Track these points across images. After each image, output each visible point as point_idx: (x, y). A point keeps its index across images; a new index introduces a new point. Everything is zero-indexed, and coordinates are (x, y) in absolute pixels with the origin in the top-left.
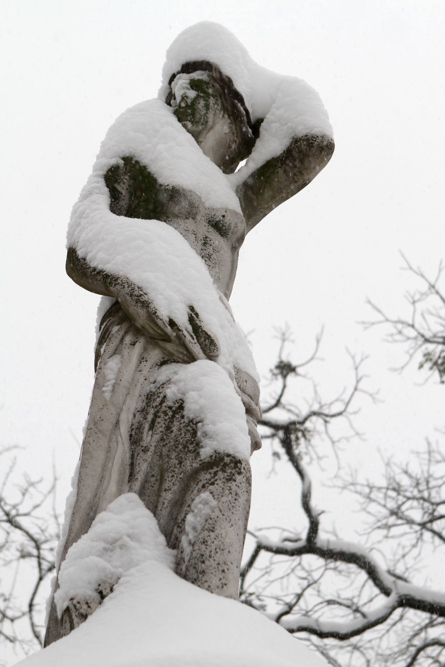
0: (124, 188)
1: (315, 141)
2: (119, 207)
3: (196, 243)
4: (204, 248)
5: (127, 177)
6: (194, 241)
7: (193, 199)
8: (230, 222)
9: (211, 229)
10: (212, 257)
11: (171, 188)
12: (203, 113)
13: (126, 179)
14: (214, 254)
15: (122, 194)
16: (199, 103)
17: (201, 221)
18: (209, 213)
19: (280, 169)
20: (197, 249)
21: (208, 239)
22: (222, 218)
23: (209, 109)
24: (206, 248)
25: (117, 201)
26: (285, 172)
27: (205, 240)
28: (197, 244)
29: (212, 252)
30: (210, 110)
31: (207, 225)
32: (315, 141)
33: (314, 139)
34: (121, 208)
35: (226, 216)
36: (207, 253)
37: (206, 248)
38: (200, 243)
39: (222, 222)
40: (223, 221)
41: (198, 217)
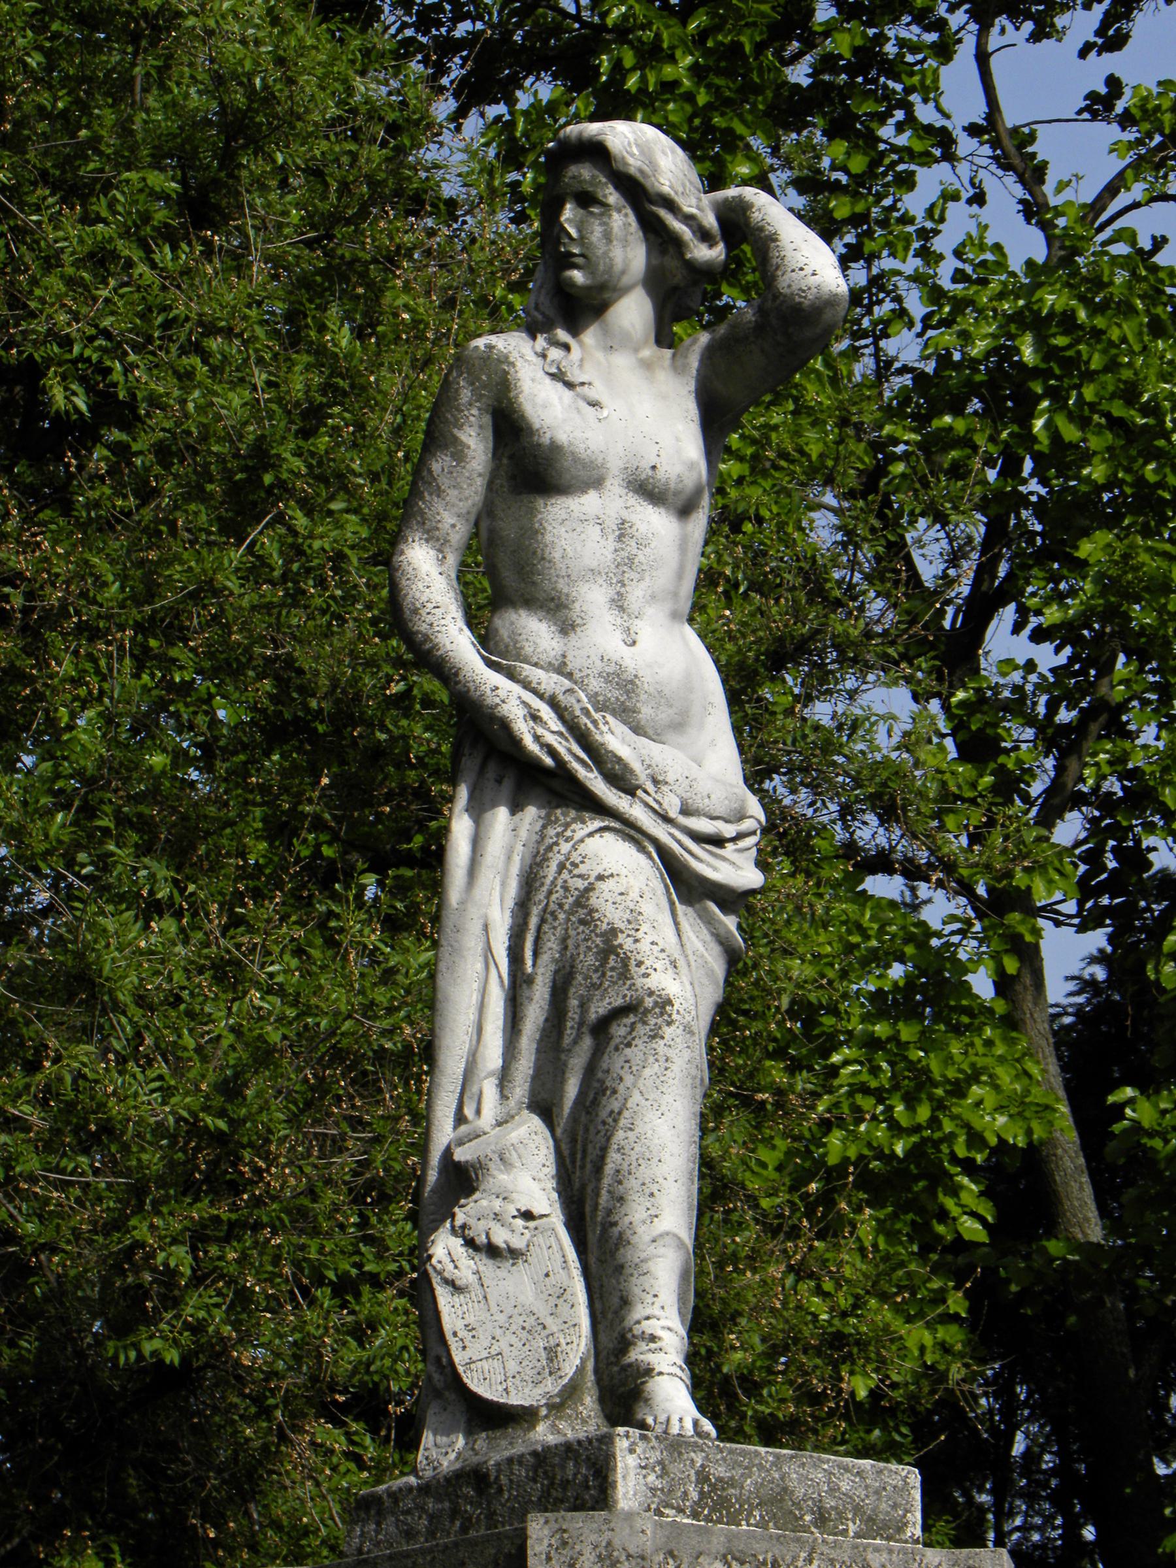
5: (474, 412)
9: (633, 500)
38: (611, 538)
41: (608, 483)
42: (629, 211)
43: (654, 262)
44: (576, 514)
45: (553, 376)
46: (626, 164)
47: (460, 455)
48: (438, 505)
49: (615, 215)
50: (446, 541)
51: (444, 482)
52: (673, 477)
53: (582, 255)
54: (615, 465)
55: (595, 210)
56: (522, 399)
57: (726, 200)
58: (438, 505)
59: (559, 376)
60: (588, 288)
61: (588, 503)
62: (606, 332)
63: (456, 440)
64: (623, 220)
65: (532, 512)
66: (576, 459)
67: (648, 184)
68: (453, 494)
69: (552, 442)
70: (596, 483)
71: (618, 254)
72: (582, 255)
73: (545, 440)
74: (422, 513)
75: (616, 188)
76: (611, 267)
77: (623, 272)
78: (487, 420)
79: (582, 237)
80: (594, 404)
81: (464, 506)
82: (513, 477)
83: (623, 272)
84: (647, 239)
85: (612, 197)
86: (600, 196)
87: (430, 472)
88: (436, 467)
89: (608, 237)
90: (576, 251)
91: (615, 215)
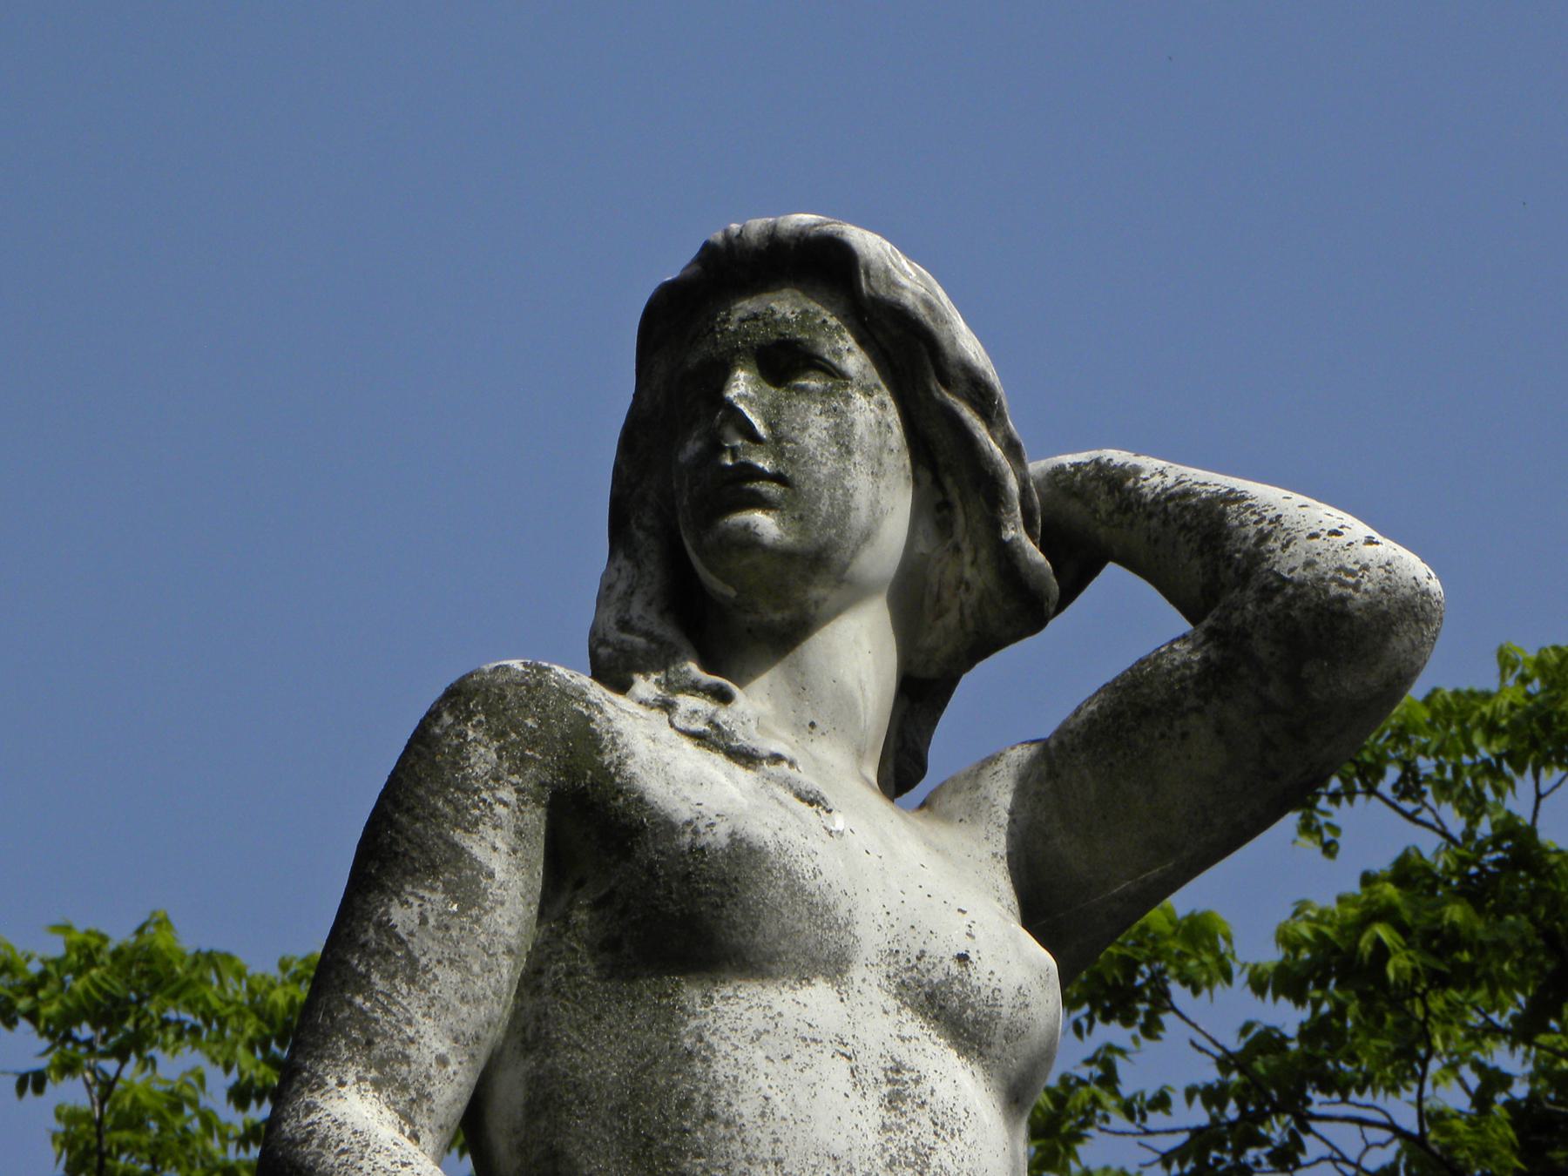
0: (499, 844)
1: (1356, 587)
2: (482, 938)
3: (855, 1097)
4: (892, 1118)
5: (507, 793)
6: (848, 1088)
7: (824, 888)
8: (993, 984)
9: (914, 1026)
10: (934, 1161)
11: (724, 841)
12: (825, 471)
13: (506, 804)
14: (941, 1144)
15: (491, 875)
16: (804, 429)
17: (864, 987)
18: (895, 947)
19: (1194, 719)
20: (864, 1126)
21: (907, 1076)
22: (955, 969)
23: (849, 452)
24: (903, 1121)
25: (475, 912)
26: (1220, 732)
27: (896, 1082)
28: (862, 1103)
29: (929, 1139)
30: (857, 457)
31: (892, 1004)
32: (1356, 587)
33: (1351, 580)
34: (491, 943)
35: (973, 956)
36: (911, 1142)
37: (903, 1121)
38: (874, 1097)
39: (957, 987)
40: (961, 981)
41: (857, 973)
43: (922, 547)
44: (789, 1022)
45: (699, 738)
47: (469, 889)
48: (411, 1002)
49: (859, 399)
50: (423, 1096)
51: (427, 948)
52: (1008, 992)
53: (779, 478)
54: (870, 938)
55: (813, 383)
56: (632, 767)
57: (1060, 470)
58: (411, 1002)
59: (712, 739)
60: (784, 555)
61: (814, 1003)
62: (801, 689)
63: (458, 851)
64: (873, 414)
65: (670, 1016)
66: (795, 889)
68: (448, 977)
69: (735, 839)
70: (832, 964)
71: (860, 482)
72: (779, 478)
73: (719, 837)
74: (364, 1019)
75: (861, 342)
76: (846, 511)
78: (536, 818)
79: (778, 439)
80: (812, 799)
81: (472, 1017)
82: (609, 945)
84: (917, 482)
85: (855, 361)
86: (825, 350)
87: (386, 928)
88: (401, 916)
89: (842, 440)
90: (765, 464)
91: (859, 399)
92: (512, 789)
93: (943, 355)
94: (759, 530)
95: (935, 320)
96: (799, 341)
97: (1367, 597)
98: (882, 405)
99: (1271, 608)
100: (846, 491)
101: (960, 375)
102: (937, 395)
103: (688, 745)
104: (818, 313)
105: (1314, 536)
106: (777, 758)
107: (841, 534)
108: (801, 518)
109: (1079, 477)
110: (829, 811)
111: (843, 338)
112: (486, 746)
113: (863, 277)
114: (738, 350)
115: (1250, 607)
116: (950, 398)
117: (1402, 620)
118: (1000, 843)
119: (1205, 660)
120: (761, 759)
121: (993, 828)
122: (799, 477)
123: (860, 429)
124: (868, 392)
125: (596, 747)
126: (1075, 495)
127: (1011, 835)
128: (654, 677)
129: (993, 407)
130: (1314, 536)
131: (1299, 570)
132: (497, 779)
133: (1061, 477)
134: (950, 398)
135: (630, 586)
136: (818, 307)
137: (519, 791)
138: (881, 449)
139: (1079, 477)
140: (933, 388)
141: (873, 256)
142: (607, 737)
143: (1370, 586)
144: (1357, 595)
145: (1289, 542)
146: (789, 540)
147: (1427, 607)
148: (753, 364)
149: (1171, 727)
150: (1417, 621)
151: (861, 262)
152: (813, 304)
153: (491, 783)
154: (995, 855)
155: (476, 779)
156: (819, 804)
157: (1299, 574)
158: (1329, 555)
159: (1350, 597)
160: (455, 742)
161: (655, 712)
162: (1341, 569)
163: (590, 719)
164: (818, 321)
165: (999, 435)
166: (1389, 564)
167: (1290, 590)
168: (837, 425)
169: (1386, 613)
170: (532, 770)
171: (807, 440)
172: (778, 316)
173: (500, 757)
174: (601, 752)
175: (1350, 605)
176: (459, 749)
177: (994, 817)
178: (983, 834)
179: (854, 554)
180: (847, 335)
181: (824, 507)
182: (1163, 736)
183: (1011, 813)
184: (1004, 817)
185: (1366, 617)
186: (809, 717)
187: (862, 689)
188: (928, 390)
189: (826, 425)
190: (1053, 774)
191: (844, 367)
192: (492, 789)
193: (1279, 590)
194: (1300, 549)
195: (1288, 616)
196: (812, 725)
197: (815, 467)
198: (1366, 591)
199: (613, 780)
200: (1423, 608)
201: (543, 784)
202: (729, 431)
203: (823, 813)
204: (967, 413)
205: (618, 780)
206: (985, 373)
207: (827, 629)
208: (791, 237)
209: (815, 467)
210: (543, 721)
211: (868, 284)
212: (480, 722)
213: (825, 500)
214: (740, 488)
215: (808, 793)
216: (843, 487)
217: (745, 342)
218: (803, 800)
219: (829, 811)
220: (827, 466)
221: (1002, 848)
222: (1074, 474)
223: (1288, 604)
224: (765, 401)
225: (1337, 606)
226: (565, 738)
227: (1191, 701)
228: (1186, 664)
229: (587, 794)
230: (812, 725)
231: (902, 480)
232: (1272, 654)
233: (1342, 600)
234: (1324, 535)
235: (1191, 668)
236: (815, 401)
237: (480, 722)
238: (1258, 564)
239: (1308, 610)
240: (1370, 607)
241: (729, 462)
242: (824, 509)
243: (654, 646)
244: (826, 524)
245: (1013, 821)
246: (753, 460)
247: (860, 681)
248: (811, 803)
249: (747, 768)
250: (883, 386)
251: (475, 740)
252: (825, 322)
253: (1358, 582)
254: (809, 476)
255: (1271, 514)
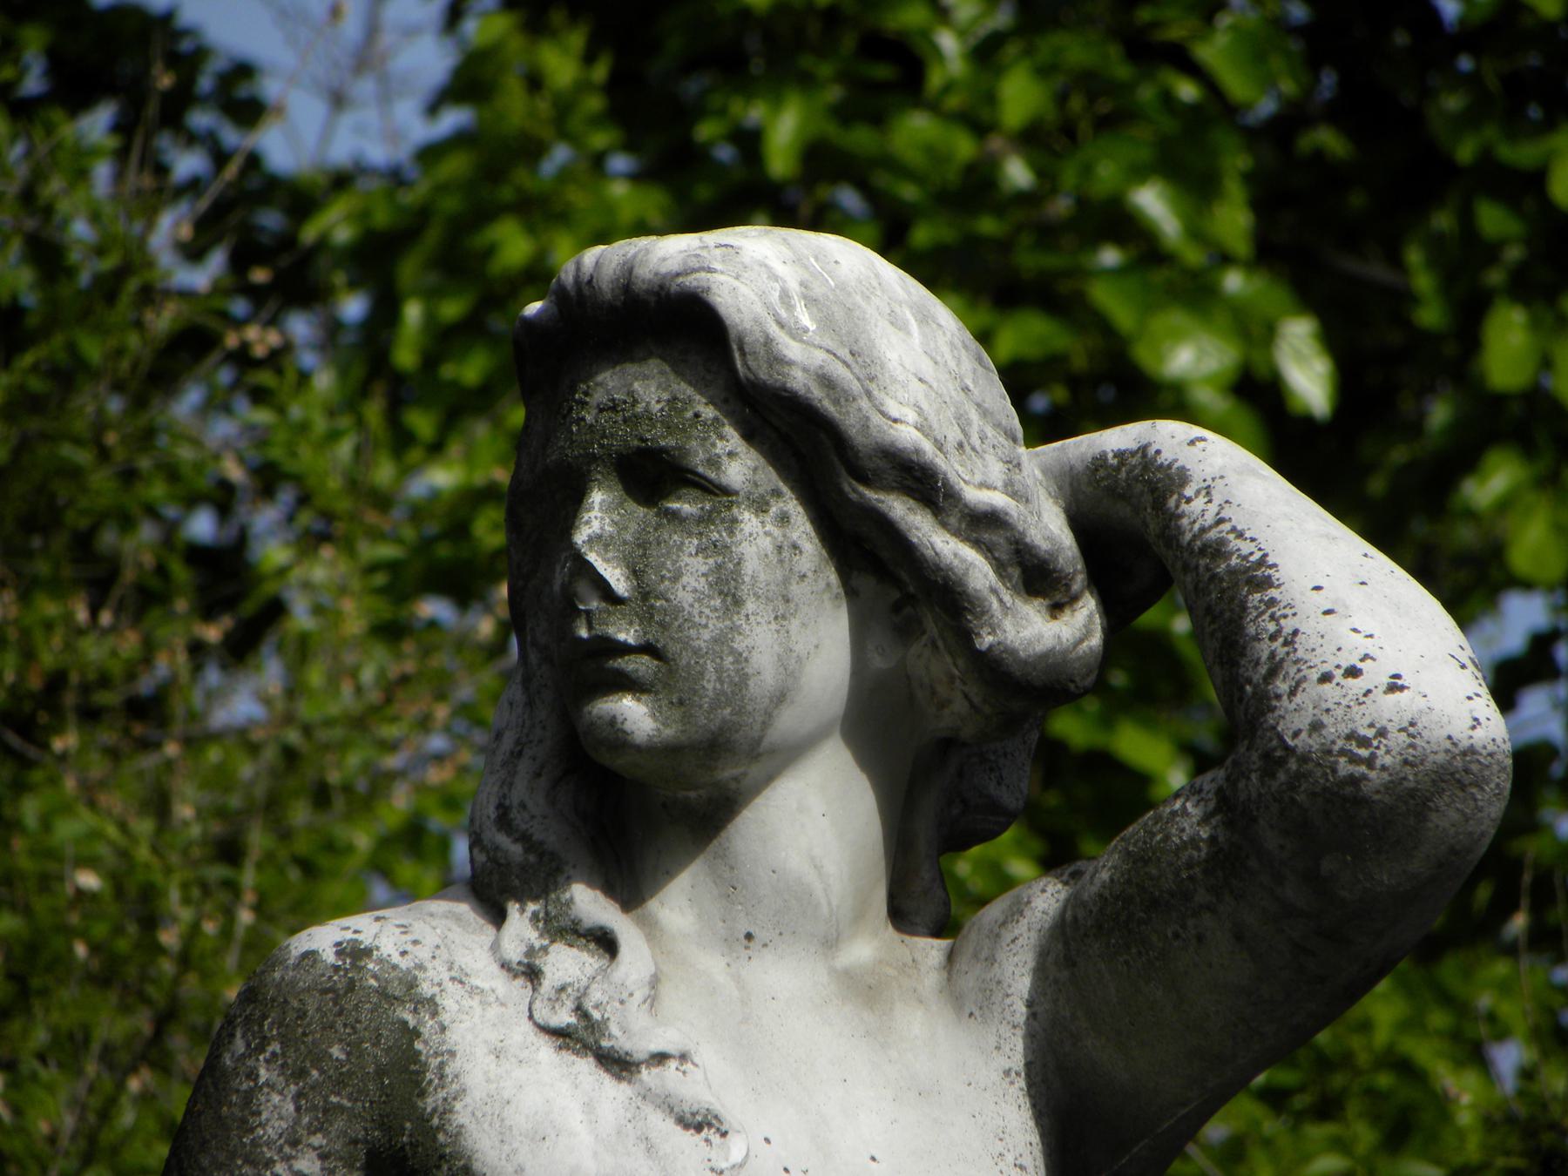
1: (1370, 762)
12: (706, 635)
16: (676, 578)
23: (738, 602)
30: (750, 606)
33: (1364, 752)
42: (792, 505)
43: (878, 662)
45: (562, 1036)
46: (777, 360)
49: (749, 521)
53: (648, 649)
55: (685, 506)
56: (462, 1115)
62: (731, 889)
64: (773, 536)
67: (849, 423)
71: (760, 642)
72: (648, 649)
75: (749, 436)
77: (781, 697)
79: (645, 593)
83: (781, 697)
85: (740, 464)
86: (697, 460)
89: (727, 587)
90: (627, 635)
91: (749, 521)
92: (314, 1155)
93: (852, 448)
94: (628, 726)
95: (836, 402)
96: (663, 450)
97: (1385, 776)
98: (784, 519)
99: (1275, 785)
100: (739, 658)
101: (882, 464)
102: (853, 496)
103: (545, 1050)
104: (690, 400)
105: (1326, 678)
106: (660, 1058)
107: (740, 711)
108: (681, 702)
109: (1123, 475)
110: (724, 1134)
111: (721, 437)
112: (281, 1093)
113: (737, 355)
114: (594, 458)
115: (1254, 777)
116: (871, 495)
117: (1441, 792)
118: (1015, 1053)
119: (1213, 840)
120: (638, 1065)
121: (1005, 1030)
122: (673, 648)
123: (751, 566)
124: (761, 507)
125: (418, 1084)
126: (1122, 497)
127: (1030, 1036)
128: (532, 907)
129: (937, 490)
130: (1326, 678)
131: (1304, 735)
132: (294, 1143)
133: (1102, 473)
134: (871, 495)
135: (518, 742)
136: (690, 391)
137: (323, 1157)
138: (786, 581)
139: (1123, 475)
140: (847, 488)
141: (747, 325)
142: (434, 1062)
143: (1388, 760)
144: (1373, 774)
145: (1298, 684)
146: (669, 733)
147: (1474, 767)
148: (614, 477)
149: (1184, 926)
150: (1463, 787)
151: (733, 335)
152: (683, 385)
153: (287, 1149)
154: (1007, 1073)
155: (268, 1144)
156: (710, 1125)
157: (1304, 742)
158: (1339, 712)
159: (1364, 777)
160: (244, 1086)
161: (520, 981)
162: (1351, 736)
163: (415, 1034)
164: (689, 414)
165: (953, 521)
166: (1412, 724)
167: (1293, 765)
168: (719, 567)
169: (1415, 790)
170: (339, 1124)
171: (681, 594)
172: (639, 408)
173: (298, 1109)
174: (422, 1094)
175: (1366, 788)
176: (248, 1098)
177: (1007, 1014)
178: (992, 1040)
179: (765, 725)
180: (729, 430)
181: (710, 684)
182: (1176, 936)
183: (1030, 1004)
184: (1021, 1010)
185: (1387, 799)
186: (743, 926)
187: (818, 868)
188: (841, 492)
189: (704, 569)
190: (1069, 962)
191: (724, 480)
192: (288, 1159)
193: (1281, 762)
194: (1313, 691)
195: (1293, 800)
196: (749, 936)
197: (692, 632)
198: (1384, 768)
199: (435, 1139)
200: (1467, 771)
201: (355, 1142)
202: (582, 587)
203: (716, 1139)
204: (899, 509)
205: (441, 1137)
206: (917, 451)
207: (759, 800)
208: (647, 292)
209: (692, 632)
210: (353, 1049)
211: (745, 364)
212: (274, 1054)
213: (711, 674)
214: (598, 668)
215: (694, 1114)
216: (732, 651)
217: (602, 446)
218: (687, 1126)
219: (724, 1134)
220: (706, 625)
221: (1017, 1061)
222: (1118, 469)
223: (1292, 786)
224: (629, 537)
225: (1349, 790)
226: (381, 1072)
227: (1202, 896)
228: (1194, 842)
229: (405, 1158)
230: (749, 936)
231: (828, 605)
232: (1282, 847)
233: (1354, 781)
234: (1338, 673)
235: (1199, 849)
236: (690, 534)
237: (274, 1054)
238: (1263, 714)
239: (1314, 794)
240: (1389, 787)
241: (584, 633)
242: (710, 686)
243: (532, 858)
244: (716, 705)
245: (1033, 1016)
246: (611, 630)
247: (812, 859)
248: (699, 1128)
249: (619, 1078)
250: (785, 489)
251: (267, 1084)
252: (697, 415)
253: (1373, 756)
254: (686, 643)
255: (1288, 625)
